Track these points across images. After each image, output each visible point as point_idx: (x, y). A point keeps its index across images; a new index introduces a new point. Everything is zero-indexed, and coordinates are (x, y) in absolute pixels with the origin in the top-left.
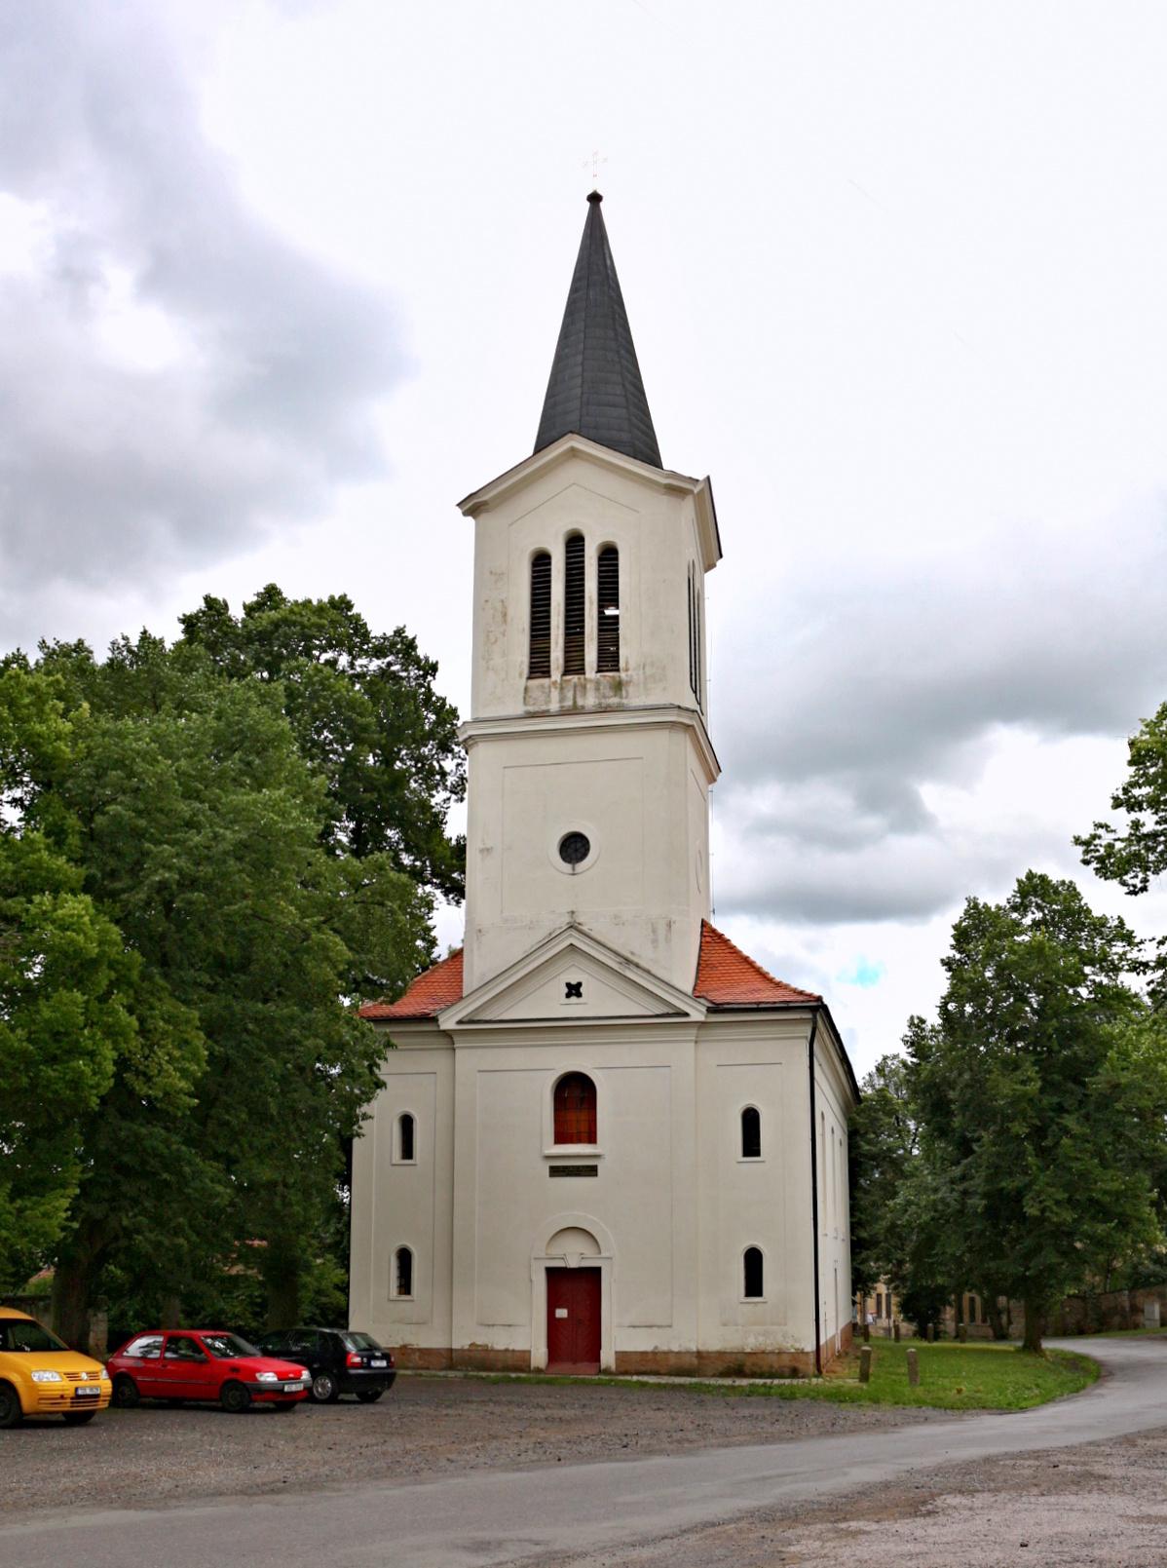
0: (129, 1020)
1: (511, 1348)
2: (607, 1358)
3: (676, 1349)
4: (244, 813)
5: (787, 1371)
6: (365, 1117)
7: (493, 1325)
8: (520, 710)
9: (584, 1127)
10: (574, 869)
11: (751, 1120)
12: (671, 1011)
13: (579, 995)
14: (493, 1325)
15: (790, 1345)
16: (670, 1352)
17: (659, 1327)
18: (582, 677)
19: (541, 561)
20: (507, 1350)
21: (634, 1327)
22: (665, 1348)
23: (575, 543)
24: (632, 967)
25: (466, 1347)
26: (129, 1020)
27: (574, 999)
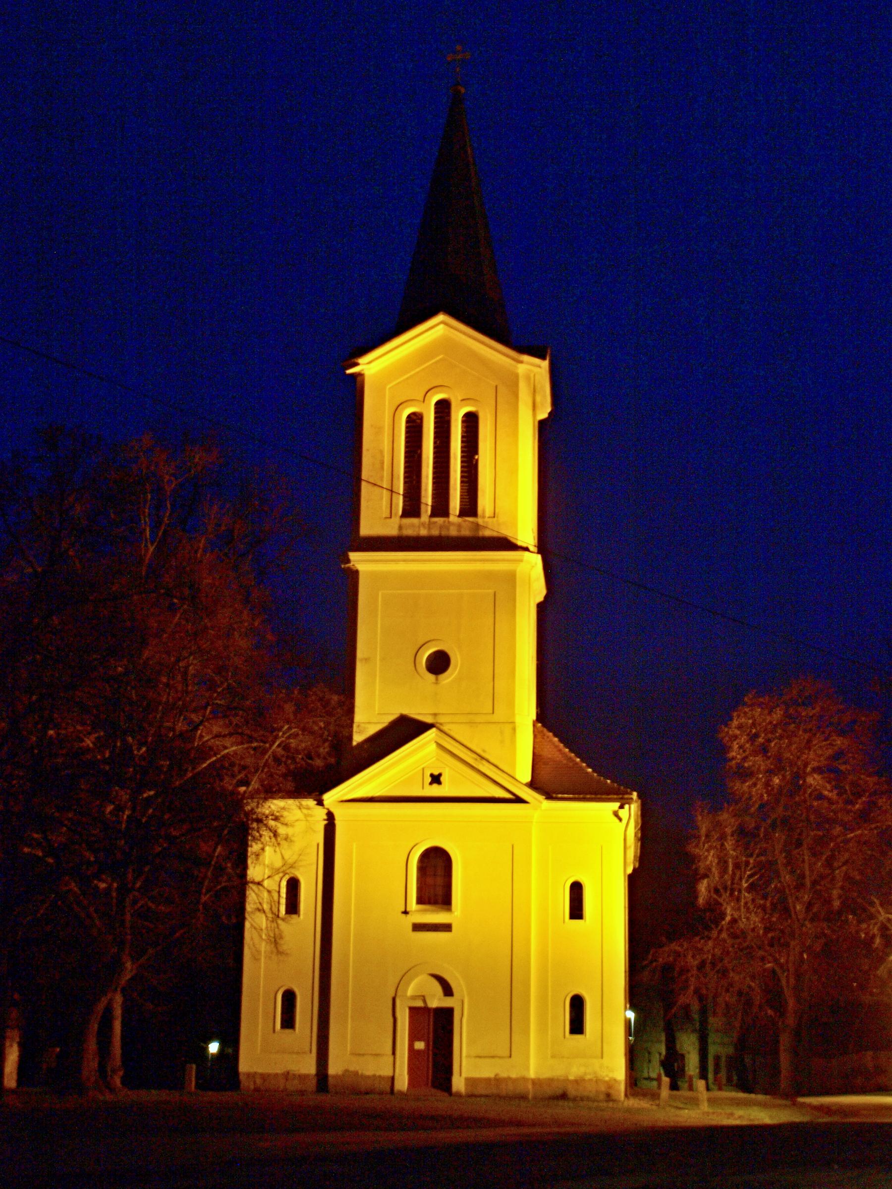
1: (378, 1074)
2: (458, 1083)
4: (152, 629)
5: (602, 1097)
6: (325, 820)
8: (386, 494)
9: (440, 891)
10: (437, 679)
11: (577, 889)
12: (508, 796)
13: (439, 783)
14: (363, 1055)
16: (509, 1078)
17: (500, 1057)
19: (415, 424)
20: (374, 1076)
21: (480, 1057)
23: (443, 408)
24: (484, 762)
25: (340, 1073)
27: (436, 773)
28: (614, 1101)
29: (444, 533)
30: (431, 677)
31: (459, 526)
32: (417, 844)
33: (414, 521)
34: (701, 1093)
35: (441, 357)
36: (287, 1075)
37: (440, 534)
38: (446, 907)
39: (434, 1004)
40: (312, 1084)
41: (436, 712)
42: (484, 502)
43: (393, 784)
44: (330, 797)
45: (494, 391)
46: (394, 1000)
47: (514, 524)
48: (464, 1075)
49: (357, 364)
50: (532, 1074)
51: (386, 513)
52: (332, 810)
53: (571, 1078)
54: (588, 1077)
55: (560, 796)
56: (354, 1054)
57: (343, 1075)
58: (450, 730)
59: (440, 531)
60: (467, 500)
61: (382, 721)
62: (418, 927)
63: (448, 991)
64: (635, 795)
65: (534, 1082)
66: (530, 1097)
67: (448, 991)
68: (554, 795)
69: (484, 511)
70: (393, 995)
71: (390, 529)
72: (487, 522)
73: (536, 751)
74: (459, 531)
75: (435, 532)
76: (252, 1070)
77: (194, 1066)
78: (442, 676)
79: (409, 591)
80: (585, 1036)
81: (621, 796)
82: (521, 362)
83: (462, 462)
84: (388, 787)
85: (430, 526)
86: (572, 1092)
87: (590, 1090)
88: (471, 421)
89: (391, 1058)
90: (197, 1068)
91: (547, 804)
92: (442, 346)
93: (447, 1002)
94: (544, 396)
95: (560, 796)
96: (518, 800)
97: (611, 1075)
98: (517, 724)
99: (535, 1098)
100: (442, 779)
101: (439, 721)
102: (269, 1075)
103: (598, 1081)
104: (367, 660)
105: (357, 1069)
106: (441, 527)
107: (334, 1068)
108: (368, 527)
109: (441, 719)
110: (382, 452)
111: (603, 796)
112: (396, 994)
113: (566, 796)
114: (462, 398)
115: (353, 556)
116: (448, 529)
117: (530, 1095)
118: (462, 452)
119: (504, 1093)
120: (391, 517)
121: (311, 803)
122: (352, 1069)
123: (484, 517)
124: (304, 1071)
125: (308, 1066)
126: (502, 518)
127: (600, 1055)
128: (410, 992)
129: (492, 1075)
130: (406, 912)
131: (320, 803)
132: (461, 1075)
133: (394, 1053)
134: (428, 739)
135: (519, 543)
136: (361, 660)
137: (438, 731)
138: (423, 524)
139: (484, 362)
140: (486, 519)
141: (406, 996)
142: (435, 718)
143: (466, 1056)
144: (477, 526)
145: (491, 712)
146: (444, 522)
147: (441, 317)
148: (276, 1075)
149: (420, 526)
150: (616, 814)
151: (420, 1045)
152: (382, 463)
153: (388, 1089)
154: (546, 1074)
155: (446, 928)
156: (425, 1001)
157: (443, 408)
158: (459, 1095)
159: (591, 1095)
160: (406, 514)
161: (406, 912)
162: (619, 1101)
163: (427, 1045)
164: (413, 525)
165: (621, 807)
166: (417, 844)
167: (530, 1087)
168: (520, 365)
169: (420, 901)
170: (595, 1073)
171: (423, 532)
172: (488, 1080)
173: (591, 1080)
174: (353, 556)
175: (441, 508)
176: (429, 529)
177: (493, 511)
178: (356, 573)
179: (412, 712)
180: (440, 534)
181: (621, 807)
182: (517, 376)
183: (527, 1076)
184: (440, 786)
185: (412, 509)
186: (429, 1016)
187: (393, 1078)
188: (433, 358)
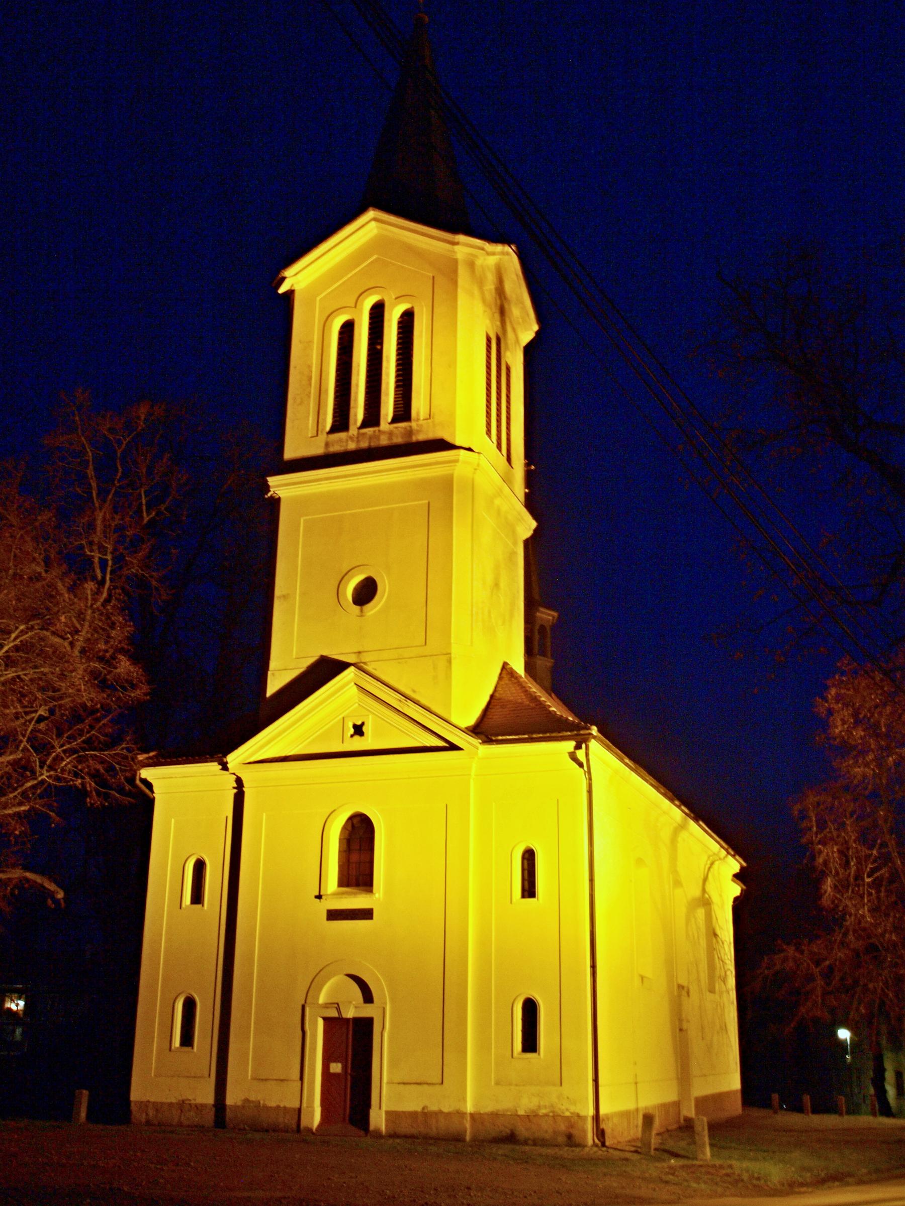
0: (505, 676)
2: (378, 1119)
3: (446, 1110)
5: (561, 1139)
6: (234, 788)
7: (266, 1080)
10: (362, 611)
12: (441, 744)
14: (266, 1080)
15: (567, 1109)
18: (376, 429)
19: (348, 330)
20: (278, 1107)
21: (404, 1084)
22: (434, 1108)
24: (410, 703)
25: (239, 1103)
26: (505, 676)
28: (578, 1145)
29: (373, 444)
30: (357, 609)
31: (390, 434)
32: (334, 811)
33: (342, 435)
34: (698, 1134)
35: (375, 257)
36: (182, 1105)
37: (370, 445)
38: (368, 888)
39: (350, 1013)
40: (209, 1118)
41: (360, 650)
42: (419, 405)
43: (308, 741)
44: (234, 759)
45: (431, 281)
46: (303, 1007)
47: (452, 424)
48: (384, 1108)
49: (284, 279)
50: (470, 1108)
51: (311, 430)
52: (239, 775)
53: (521, 1112)
54: (543, 1111)
55: (500, 738)
56: (254, 1079)
57: (243, 1107)
58: (375, 669)
59: (370, 443)
60: (402, 405)
61: (301, 666)
62: (334, 915)
63: (368, 997)
64: (594, 730)
65: (475, 1117)
66: (468, 1138)
67: (368, 997)
68: (494, 738)
69: (418, 414)
70: (303, 1002)
71: (316, 449)
72: (422, 425)
73: (497, 695)
74: (390, 438)
75: (364, 444)
76: (144, 1099)
77: (86, 1093)
78: (367, 607)
79: (328, 515)
80: (539, 1054)
81: (575, 732)
82: (457, 244)
83: (398, 365)
84: (300, 746)
85: (358, 438)
86: (522, 1132)
87: (546, 1129)
88: (407, 322)
89: (299, 1083)
90: (91, 1097)
91: (486, 750)
92: (378, 245)
93: (367, 1011)
94: (524, 308)
95: (500, 738)
96: (453, 747)
97: (573, 1109)
98: (453, 655)
99: (474, 1139)
100: (364, 729)
101: (363, 660)
102: (162, 1104)
103: (555, 1116)
104: (285, 597)
105: (259, 1098)
106: (371, 438)
107: (232, 1098)
108: (290, 452)
109: (365, 658)
110: (310, 367)
111: (554, 735)
112: (305, 1002)
113: (508, 737)
114: (397, 296)
115: (272, 481)
116: (379, 439)
117: (468, 1132)
118: (398, 354)
119: (433, 1132)
120: (317, 435)
121: (214, 767)
122: (253, 1098)
123: (418, 420)
124: (200, 1100)
125: (206, 1095)
126: (438, 418)
127: (559, 1083)
128: (322, 1000)
129: (419, 1109)
130: (319, 897)
131: (225, 767)
132: (380, 1108)
133: (301, 1078)
134: (345, 680)
135: (458, 443)
136: (279, 597)
137: (357, 669)
138: (351, 438)
139: (410, 249)
140: (421, 422)
141: (318, 1004)
142: (358, 657)
143: (388, 1083)
144: (410, 432)
145: (424, 644)
146: (374, 432)
147: (371, 214)
148: (171, 1105)
149: (346, 442)
150: (573, 757)
151: (336, 1068)
152: (310, 379)
153: (294, 1126)
154: (488, 1107)
155: (366, 914)
156: (338, 1010)
157: (378, 313)
158: (378, 1135)
159: (547, 1136)
160: (334, 429)
161: (319, 897)
162: (584, 1146)
163: (345, 1068)
164: (340, 440)
165: (578, 747)
166: (334, 811)
167: (468, 1125)
168: (456, 248)
169: (341, 884)
170: (552, 1106)
171: (352, 446)
172: (413, 1115)
173: (546, 1115)
174: (272, 481)
175: (372, 417)
176: (358, 441)
177: (428, 412)
178: (275, 503)
179: (332, 653)
180: (370, 445)
181: (578, 747)
182: (456, 262)
183: (463, 1110)
184: (363, 737)
185: (341, 422)
186: (348, 1029)
187: (300, 1110)
188: (365, 259)
